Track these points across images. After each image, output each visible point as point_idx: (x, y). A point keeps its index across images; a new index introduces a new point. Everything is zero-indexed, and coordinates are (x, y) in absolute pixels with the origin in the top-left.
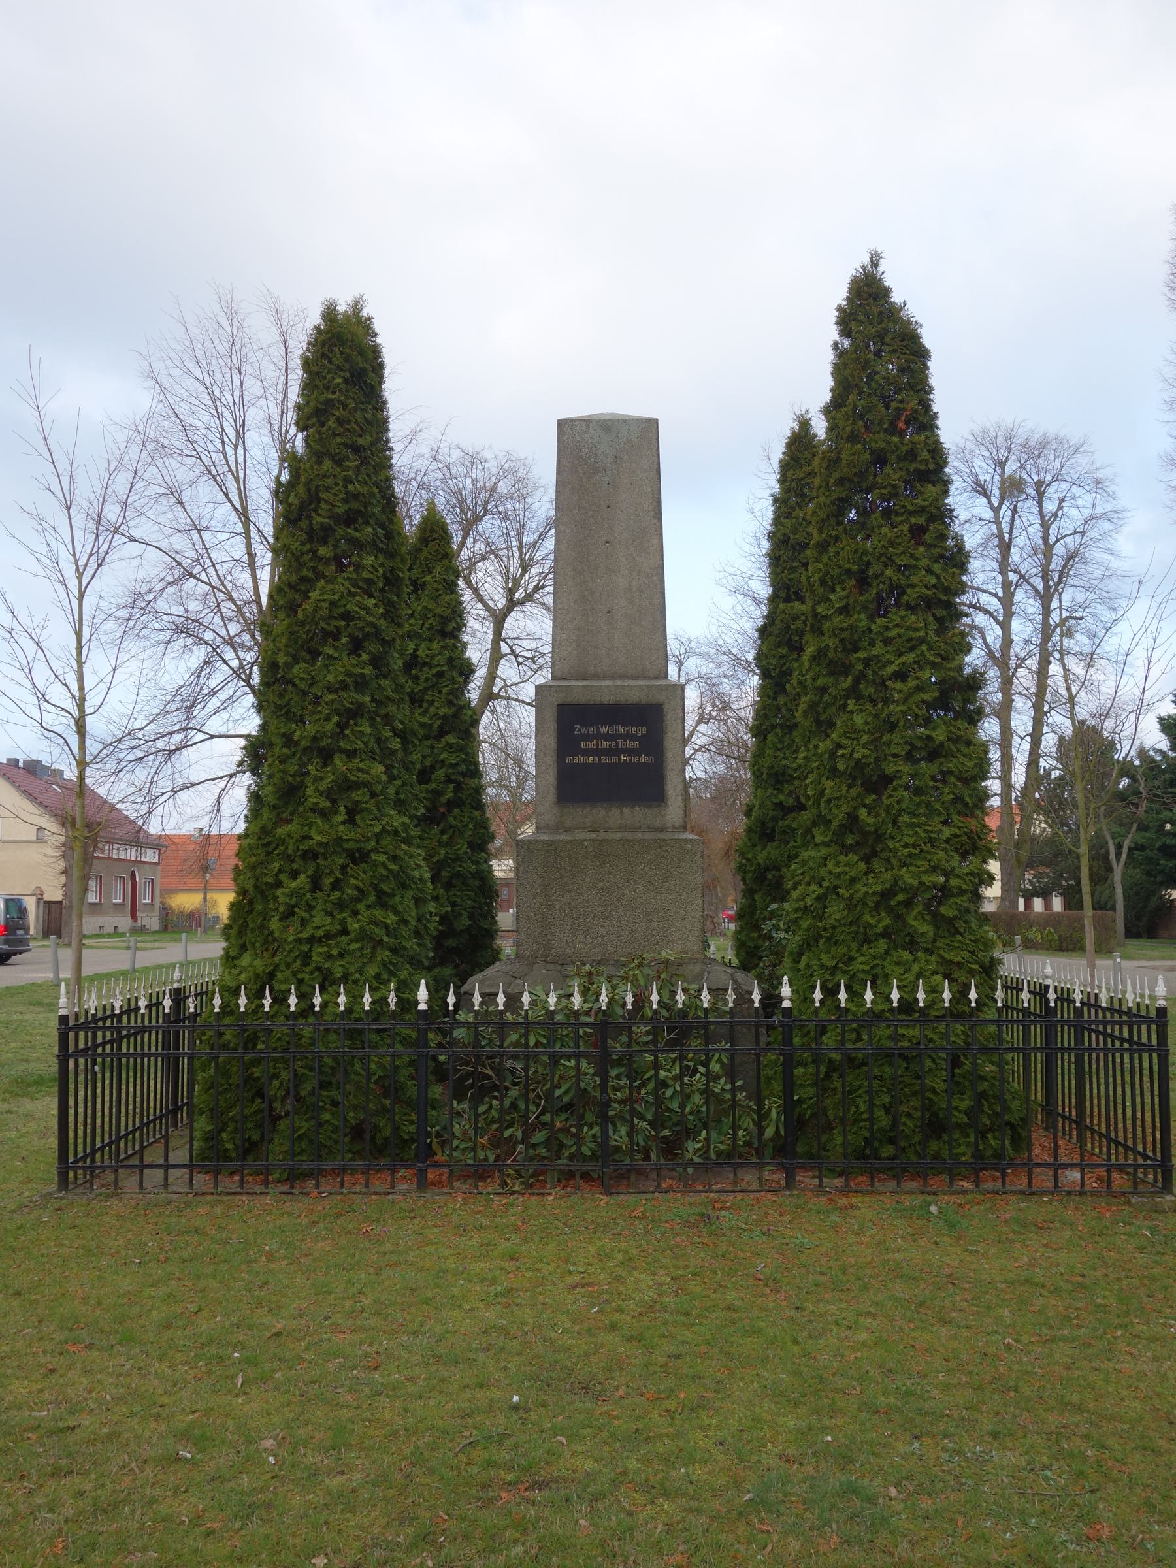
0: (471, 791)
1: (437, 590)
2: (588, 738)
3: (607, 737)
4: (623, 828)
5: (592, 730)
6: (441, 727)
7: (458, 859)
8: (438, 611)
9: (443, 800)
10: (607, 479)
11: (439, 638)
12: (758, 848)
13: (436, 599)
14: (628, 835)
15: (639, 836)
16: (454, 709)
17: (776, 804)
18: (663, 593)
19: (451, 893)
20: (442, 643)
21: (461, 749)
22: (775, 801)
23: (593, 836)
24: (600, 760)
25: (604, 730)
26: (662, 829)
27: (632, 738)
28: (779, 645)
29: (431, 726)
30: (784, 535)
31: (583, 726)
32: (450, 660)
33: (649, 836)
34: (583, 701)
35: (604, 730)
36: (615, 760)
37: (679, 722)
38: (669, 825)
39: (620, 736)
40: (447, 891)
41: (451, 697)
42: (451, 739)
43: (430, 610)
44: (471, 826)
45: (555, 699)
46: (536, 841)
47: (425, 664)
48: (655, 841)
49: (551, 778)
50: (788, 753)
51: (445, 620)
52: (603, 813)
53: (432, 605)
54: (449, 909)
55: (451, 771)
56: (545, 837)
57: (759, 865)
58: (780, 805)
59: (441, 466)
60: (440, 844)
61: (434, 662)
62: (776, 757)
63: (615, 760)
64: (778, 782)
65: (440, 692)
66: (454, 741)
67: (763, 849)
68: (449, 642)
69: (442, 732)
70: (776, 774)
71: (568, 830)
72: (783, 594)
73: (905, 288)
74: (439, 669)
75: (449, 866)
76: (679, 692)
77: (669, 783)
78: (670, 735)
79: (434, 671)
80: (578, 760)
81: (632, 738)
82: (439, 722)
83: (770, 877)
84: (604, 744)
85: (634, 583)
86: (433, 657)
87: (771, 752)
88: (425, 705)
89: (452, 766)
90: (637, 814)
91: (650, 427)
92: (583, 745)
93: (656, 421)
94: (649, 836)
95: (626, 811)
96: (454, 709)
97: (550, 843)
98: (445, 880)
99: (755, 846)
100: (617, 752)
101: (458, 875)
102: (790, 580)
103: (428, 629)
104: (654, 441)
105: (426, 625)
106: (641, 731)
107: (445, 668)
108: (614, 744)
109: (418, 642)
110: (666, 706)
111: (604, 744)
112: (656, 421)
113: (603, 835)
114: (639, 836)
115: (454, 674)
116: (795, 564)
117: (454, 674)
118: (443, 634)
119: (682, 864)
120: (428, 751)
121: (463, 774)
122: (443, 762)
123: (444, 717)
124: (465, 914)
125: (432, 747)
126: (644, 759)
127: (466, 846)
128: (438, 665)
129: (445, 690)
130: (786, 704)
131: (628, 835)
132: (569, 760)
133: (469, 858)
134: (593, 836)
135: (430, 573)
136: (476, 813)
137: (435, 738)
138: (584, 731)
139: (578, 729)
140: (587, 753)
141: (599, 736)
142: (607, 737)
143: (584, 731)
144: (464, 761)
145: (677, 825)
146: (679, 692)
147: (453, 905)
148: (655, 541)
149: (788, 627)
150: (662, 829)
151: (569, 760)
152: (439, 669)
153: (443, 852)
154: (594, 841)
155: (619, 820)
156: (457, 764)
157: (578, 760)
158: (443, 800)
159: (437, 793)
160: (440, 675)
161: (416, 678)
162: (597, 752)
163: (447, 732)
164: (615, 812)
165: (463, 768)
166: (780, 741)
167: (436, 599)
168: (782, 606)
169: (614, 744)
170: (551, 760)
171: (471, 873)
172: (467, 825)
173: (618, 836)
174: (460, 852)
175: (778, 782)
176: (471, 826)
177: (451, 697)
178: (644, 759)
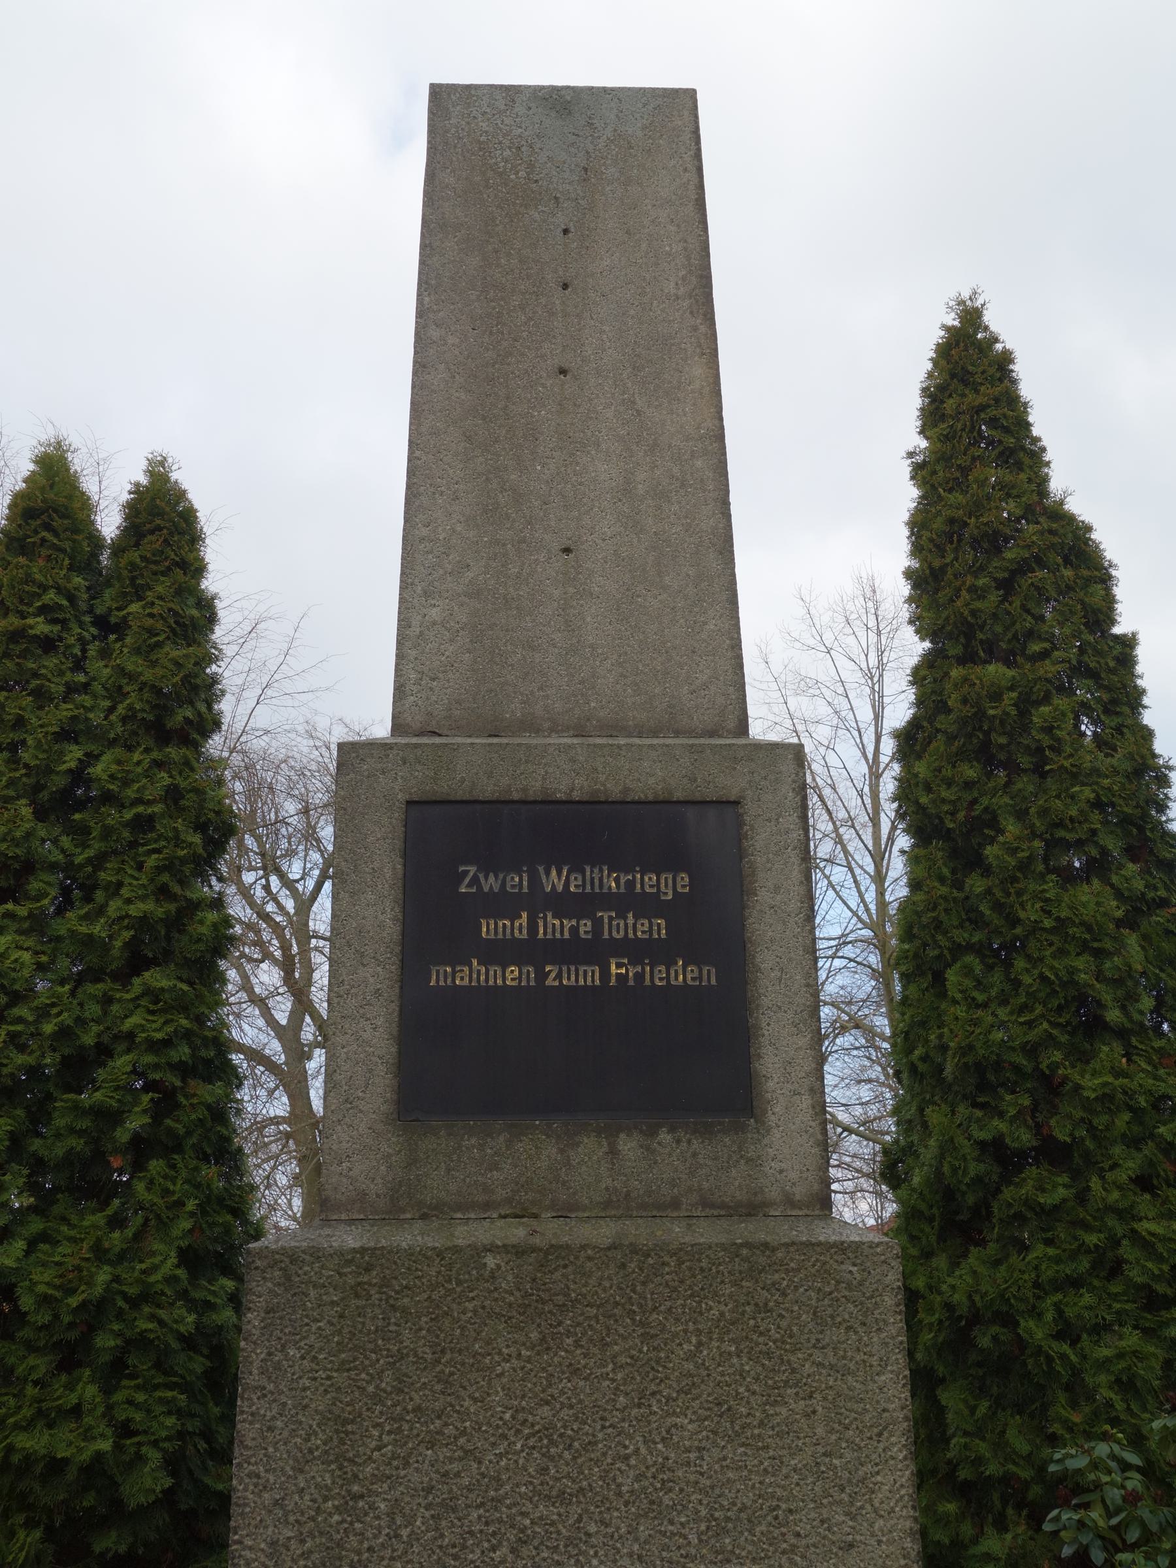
0: (201, 1113)
1: (152, 632)
2: (502, 905)
3: (563, 904)
4: (617, 1205)
5: (517, 881)
6: (133, 946)
7: (146, 1296)
8: (148, 675)
9: (122, 1135)
10: (561, 220)
11: (147, 741)
12: (941, 1262)
13: (147, 651)
14: (638, 1231)
15: (676, 1232)
16: (172, 907)
17: (982, 1145)
18: (725, 504)
19: (119, 1397)
20: (155, 755)
21: (183, 1006)
22: (983, 1135)
23: (517, 1233)
24: (542, 976)
25: (554, 880)
26: (753, 1208)
27: (647, 905)
28: (961, 756)
29: (106, 948)
30: (951, 521)
31: (487, 867)
32: (173, 795)
33: (709, 1233)
34: (488, 789)
35: (554, 880)
36: (590, 976)
37: (794, 858)
38: (773, 1193)
39: (606, 900)
40: (107, 1391)
41: (165, 878)
42: (156, 978)
43: (132, 677)
44: (191, 1205)
45: (401, 784)
46: (316, 1253)
47: (108, 798)
48: (733, 1250)
49: (377, 1034)
50: (1003, 1013)
51: (162, 703)
52: (551, 1150)
53: (133, 664)
54: (105, 1445)
55: (149, 1059)
56: (350, 1239)
57: (949, 1307)
58: (995, 1149)
59: (318, 744)
60: (100, 1254)
61: (130, 793)
62: (976, 1023)
63: (590, 976)
64: (983, 1086)
65: (140, 867)
66: (165, 983)
67: (954, 1265)
68: (174, 752)
69: (137, 963)
70: (980, 1068)
71: (427, 1213)
72: (955, 650)
73: (1004, 324)
74: (140, 809)
75: (120, 1315)
76: (787, 767)
77: (767, 1051)
78: (764, 896)
79: (128, 815)
80: (470, 974)
81: (647, 905)
82: (127, 935)
83: (985, 1342)
84: (553, 926)
85: (641, 476)
86: (126, 783)
87: (960, 1011)
88: (99, 895)
89: (154, 1046)
90: (662, 1158)
91: (668, 119)
92: (487, 929)
93: (691, 94)
94: (709, 1233)
95: (628, 1145)
96: (172, 907)
97: (364, 1260)
98: (106, 1358)
99: (928, 1255)
100: (595, 951)
101: (141, 1342)
102: (973, 613)
103: (124, 720)
104: (687, 136)
105: (121, 709)
106: (672, 885)
107: (158, 808)
108: (585, 926)
109: (93, 748)
110: (750, 810)
111: (553, 926)
112: (691, 94)
113: (551, 1230)
114: (676, 1232)
115: (179, 824)
116: (981, 582)
117: (179, 824)
118: (163, 735)
119: (832, 1335)
120: (94, 1009)
121: (184, 1070)
122: (131, 1035)
123: (144, 921)
124: (154, 1456)
125: (107, 1000)
126: (683, 974)
127: (173, 1260)
128: (139, 801)
129: (151, 861)
130: (989, 891)
131: (638, 1231)
132: (439, 976)
133: (184, 1295)
134: (517, 1233)
135: (140, 599)
136: (209, 1172)
137: (116, 976)
138: (491, 883)
139: (473, 879)
140: (499, 953)
141: (539, 902)
142: (563, 904)
143: (491, 883)
144: (188, 1035)
145: (799, 1192)
146: (787, 767)
147: (125, 1430)
148: (698, 370)
149: (980, 714)
150: (753, 1208)
151: (439, 976)
152: (140, 809)
153: (103, 1276)
154: (519, 1251)
155: (607, 1176)
156: (167, 1043)
157: (470, 974)
158: (122, 1135)
159: (109, 1117)
160: (143, 824)
161: (81, 833)
162: (532, 951)
163: (149, 964)
164: (590, 1147)
165: (183, 1052)
166: (979, 985)
167: (147, 651)
168: (956, 673)
169: (585, 926)
170: (379, 975)
171: (181, 1338)
172: (180, 1204)
173: (603, 1233)
174: (157, 1277)
175: (983, 1086)
176: (191, 1205)
177: (165, 878)
178: (683, 974)
